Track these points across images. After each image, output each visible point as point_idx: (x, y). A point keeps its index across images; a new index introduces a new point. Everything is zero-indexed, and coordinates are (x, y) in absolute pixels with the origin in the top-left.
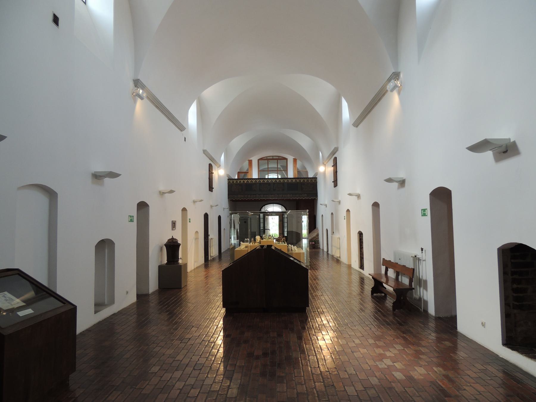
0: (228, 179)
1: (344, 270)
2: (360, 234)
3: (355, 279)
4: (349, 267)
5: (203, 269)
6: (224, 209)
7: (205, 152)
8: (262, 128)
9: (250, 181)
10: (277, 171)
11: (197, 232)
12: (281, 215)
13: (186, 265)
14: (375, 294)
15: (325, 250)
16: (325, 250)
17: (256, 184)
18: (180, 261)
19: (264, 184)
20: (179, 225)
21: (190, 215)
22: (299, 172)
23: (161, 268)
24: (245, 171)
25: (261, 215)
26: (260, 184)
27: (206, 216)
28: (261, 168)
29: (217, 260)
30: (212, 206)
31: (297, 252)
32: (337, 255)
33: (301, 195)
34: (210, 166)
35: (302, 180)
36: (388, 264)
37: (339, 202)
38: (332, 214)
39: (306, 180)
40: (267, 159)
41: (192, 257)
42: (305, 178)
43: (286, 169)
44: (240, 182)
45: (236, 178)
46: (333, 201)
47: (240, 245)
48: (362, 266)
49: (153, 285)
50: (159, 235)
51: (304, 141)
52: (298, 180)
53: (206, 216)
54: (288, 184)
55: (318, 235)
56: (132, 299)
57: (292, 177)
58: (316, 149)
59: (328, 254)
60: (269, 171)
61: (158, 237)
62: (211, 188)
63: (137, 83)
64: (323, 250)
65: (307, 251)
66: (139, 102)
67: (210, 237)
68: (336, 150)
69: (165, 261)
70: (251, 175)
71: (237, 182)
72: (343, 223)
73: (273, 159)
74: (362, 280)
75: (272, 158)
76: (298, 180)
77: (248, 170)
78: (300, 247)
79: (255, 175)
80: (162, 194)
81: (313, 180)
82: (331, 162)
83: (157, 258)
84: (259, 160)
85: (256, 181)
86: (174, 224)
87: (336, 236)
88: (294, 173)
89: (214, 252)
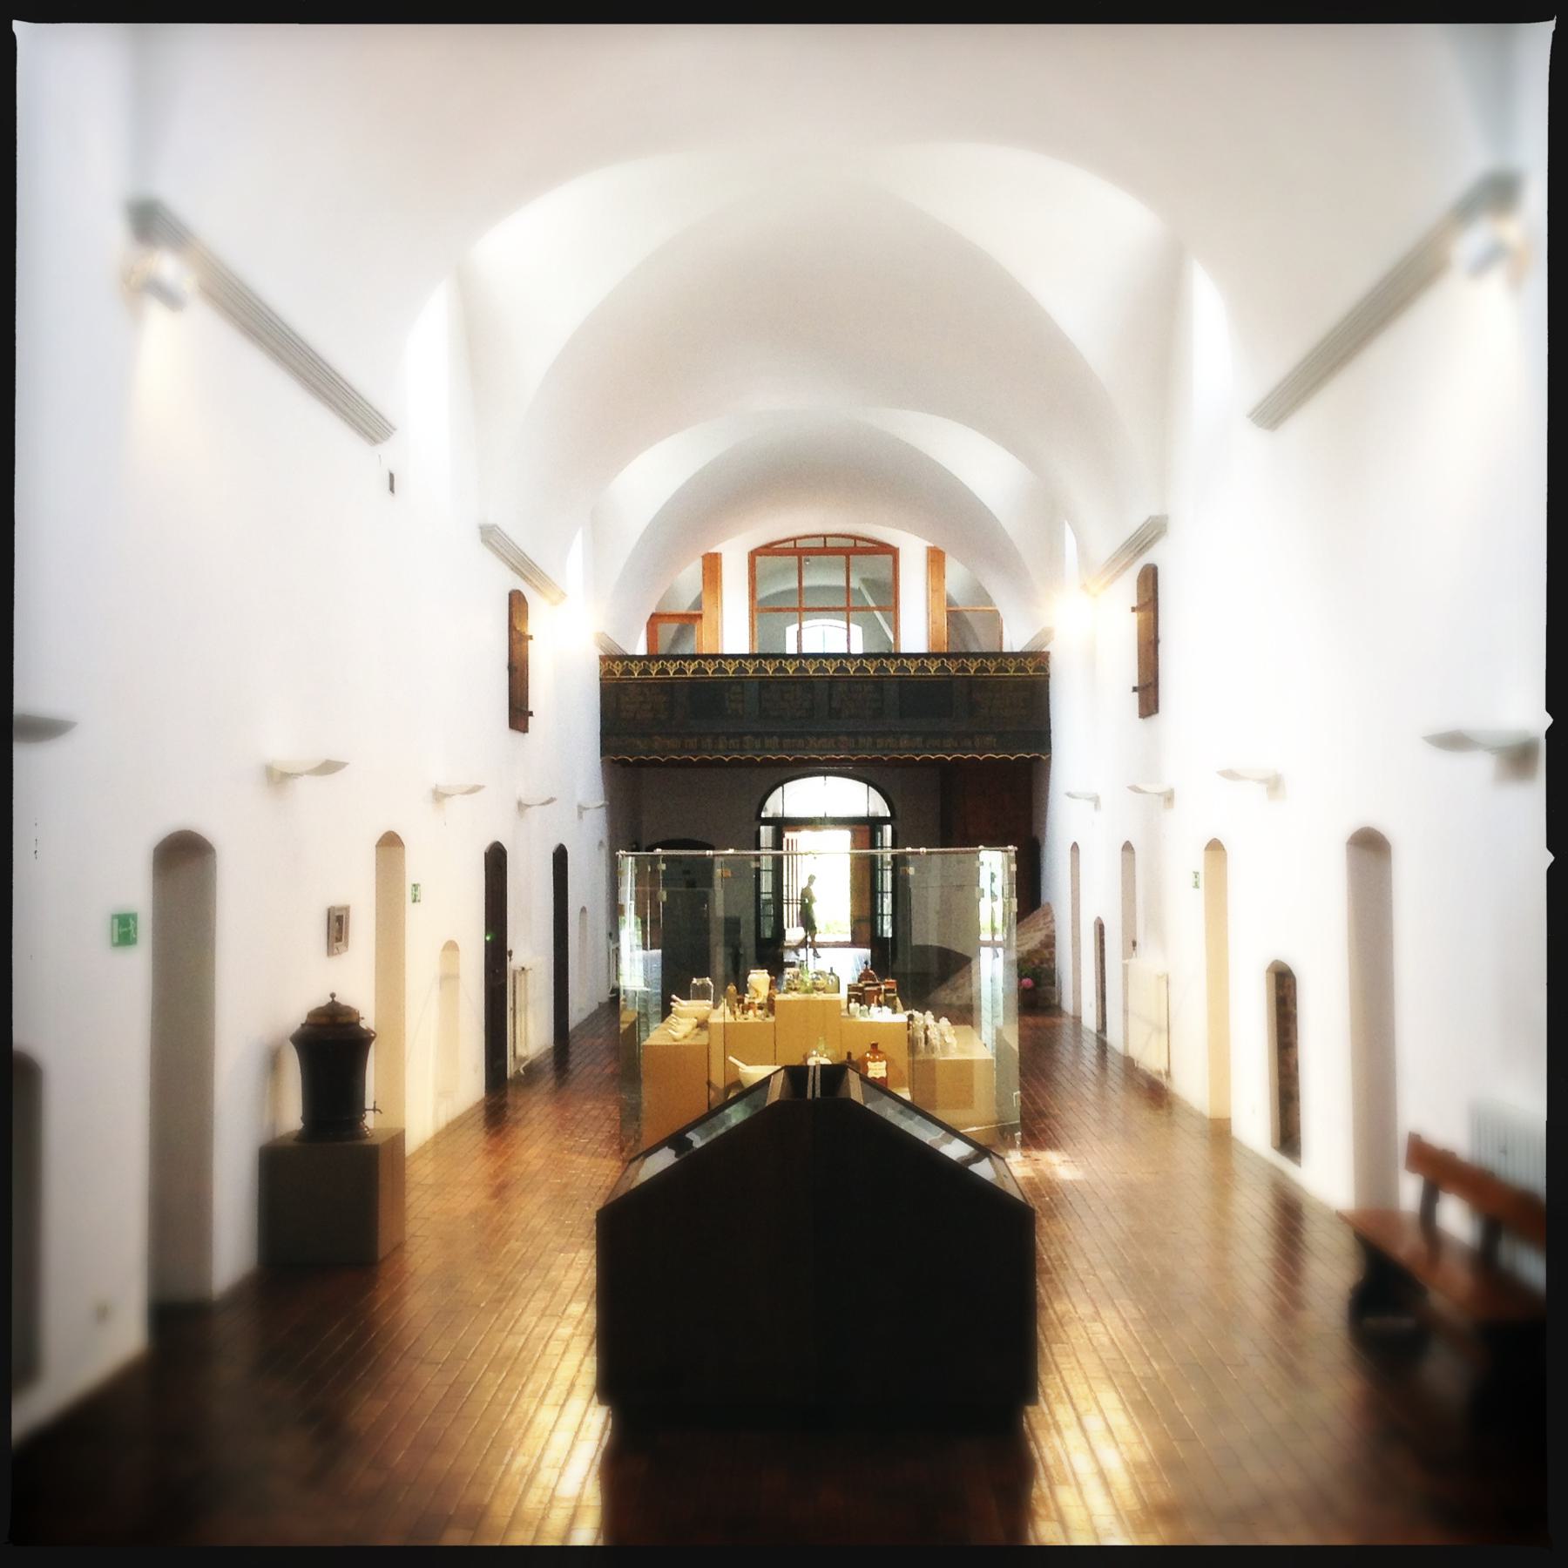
0: (603, 659)
1: (1191, 1154)
2: (1283, 985)
3: (1252, 1213)
4: (1220, 1133)
5: (476, 1137)
6: (582, 809)
7: (491, 536)
8: (779, 403)
9: (710, 668)
10: (846, 606)
11: (451, 946)
12: (865, 829)
13: (398, 1139)
14: (1371, 1322)
15: (1090, 1020)
16: (1090, 1020)
17: (740, 681)
18: (370, 1121)
19: (784, 683)
20: (362, 929)
21: (416, 865)
22: (955, 618)
23: (277, 1166)
24: (683, 610)
25: (766, 832)
26: (765, 683)
27: (496, 860)
28: (760, 595)
29: (547, 1082)
30: (522, 806)
31: (954, 1056)
32: (1151, 1059)
33: (964, 750)
34: (517, 602)
35: (973, 667)
36: (1441, 1171)
37: (1169, 798)
38: (1128, 847)
39: (992, 665)
40: (798, 551)
41: (424, 1087)
42: (987, 656)
43: (888, 595)
44: (664, 671)
45: (641, 650)
46: (1135, 789)
47: (666, 1011)
48: (1288, 1138)
49: (231, 1248)
50: (263, 991)
51: (983, 467)
52: (952, 667)
53: (496, 860)
54: (904, 682)
55: (1049, 943)
56: (124, 1337)
57: (923, 649)
58: (1049, 509)
59: (1103, 1046)
60: (801, 606)
61: (257, 1005)
62: (519, 716)
63: (149, 221)
64: (1077, 1020)
65: (1001, 1048)
66: (158, 318)
67: (513, 964)
68: (1150, 534)
69: (292, 1117)
70: (716, 631)
71: (645, 671)
72: (1184, 908)
73: (825, 551)
74: (1289, 1214)
75: (818, 543)
76: (952, 667)
77: (698, 603)
78: (965, 1015)
79: (732, 633)
80: (277, 778)
81: (1030, 665)
82: (1126, 590)
83: (251, 1105)
84: (754, 554)
85: (741, 669)
86: (337, 926)
87: (1148, 962)
88: (933, 637)
89: (532, 1034)
